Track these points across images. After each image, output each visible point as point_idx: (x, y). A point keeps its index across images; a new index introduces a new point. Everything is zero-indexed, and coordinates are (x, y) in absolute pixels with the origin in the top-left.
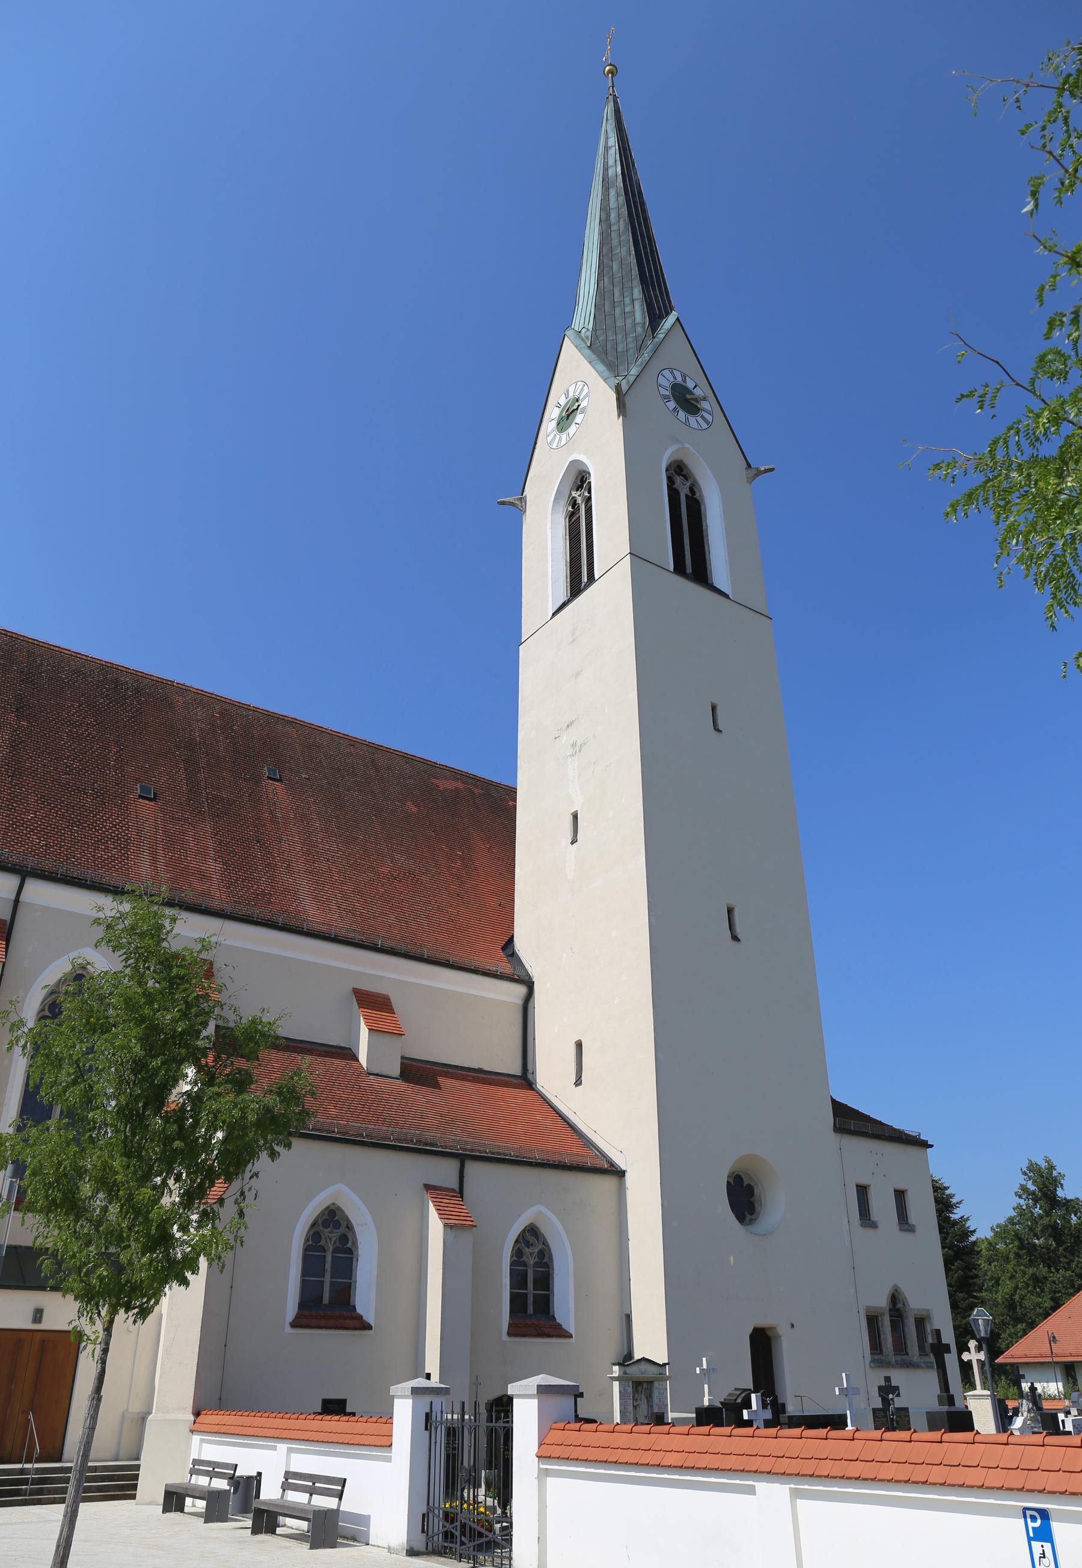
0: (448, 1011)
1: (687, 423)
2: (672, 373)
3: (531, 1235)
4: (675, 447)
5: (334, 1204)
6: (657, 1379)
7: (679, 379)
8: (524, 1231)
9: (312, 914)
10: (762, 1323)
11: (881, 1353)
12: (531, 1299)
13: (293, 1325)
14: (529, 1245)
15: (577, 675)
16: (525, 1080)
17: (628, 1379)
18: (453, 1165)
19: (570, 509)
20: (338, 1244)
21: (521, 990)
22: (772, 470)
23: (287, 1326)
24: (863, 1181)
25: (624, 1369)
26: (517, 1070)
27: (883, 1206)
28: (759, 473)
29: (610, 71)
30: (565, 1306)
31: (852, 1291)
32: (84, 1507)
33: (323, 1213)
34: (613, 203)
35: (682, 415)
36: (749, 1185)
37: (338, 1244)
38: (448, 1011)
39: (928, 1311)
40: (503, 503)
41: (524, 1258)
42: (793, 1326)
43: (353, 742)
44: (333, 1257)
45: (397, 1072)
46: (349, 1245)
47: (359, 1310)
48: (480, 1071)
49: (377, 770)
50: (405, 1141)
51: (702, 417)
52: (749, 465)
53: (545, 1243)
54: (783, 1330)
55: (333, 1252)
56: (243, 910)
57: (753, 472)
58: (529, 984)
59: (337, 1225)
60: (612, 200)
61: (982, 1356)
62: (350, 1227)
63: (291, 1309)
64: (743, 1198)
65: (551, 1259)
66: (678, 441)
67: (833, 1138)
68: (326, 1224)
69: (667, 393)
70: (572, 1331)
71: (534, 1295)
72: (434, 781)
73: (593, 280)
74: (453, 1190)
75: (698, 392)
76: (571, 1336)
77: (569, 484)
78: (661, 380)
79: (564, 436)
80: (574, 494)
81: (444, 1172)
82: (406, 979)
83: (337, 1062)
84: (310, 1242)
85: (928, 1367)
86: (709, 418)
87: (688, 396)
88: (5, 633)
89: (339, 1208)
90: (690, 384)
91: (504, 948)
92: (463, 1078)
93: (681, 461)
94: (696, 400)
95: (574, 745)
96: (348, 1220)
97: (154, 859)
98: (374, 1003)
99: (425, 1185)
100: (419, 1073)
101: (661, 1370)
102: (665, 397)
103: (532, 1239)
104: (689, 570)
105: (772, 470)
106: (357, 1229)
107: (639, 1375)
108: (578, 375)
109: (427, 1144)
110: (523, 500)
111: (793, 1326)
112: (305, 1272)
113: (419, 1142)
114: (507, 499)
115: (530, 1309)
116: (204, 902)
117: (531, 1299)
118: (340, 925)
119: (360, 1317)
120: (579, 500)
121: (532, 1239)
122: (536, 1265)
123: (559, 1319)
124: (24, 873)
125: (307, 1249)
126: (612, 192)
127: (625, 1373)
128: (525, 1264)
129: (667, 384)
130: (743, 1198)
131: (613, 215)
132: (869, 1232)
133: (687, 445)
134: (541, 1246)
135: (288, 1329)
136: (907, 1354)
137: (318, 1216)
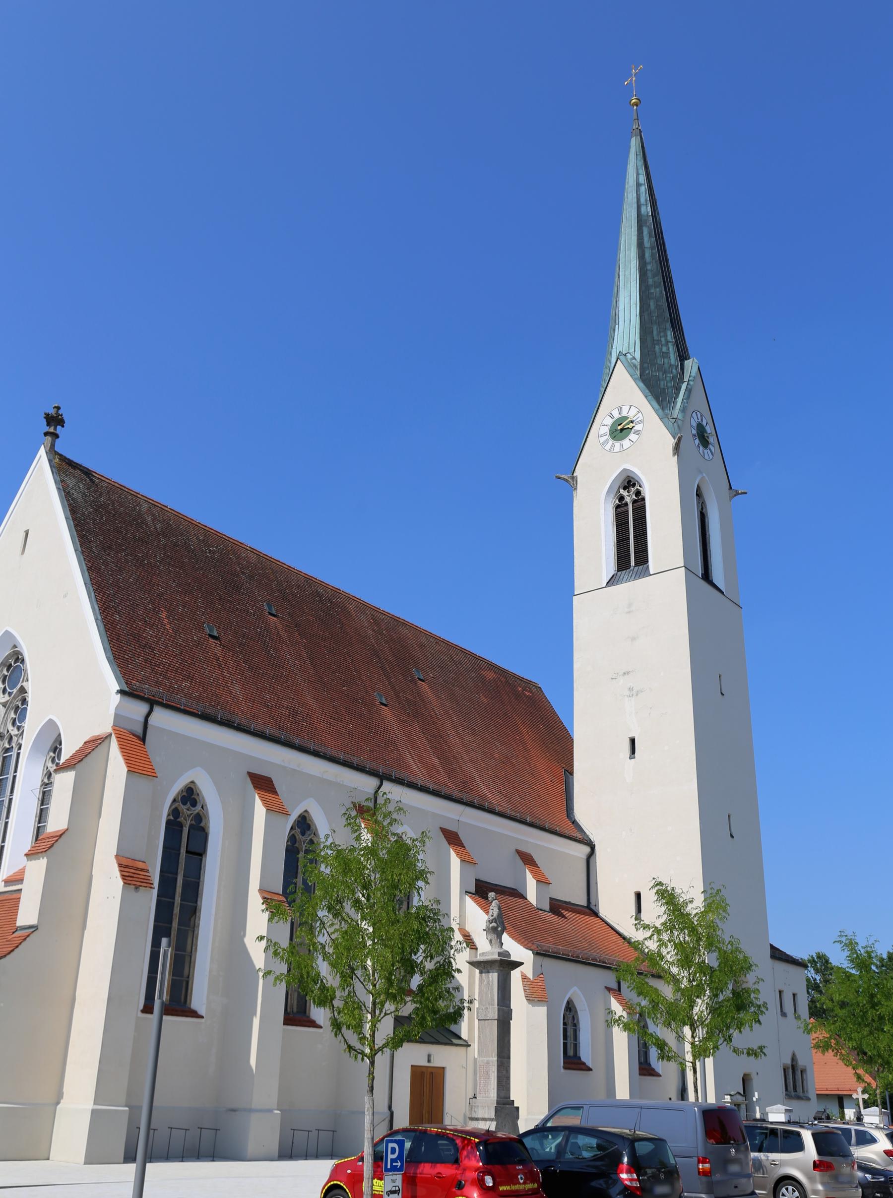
2: (702, 416)
9: (495, 800)
10: (747, 1071)
15: (633, 639)
16: (590, 910)
19: (617, 502)
21: (587, 850)
24: (781, 989)
26: (584, 903)
28: (737, 494)
32: (148, 1165)
34: (647, 244)
40: (559, 478)
45: (547, 908)
52: (731, 488)
54: (754, 1076)
58: (593, 848)
60: (646, 239)
63: (141, 1007)
73: (635, 310)
74: (614, 990)
77: (618, 484)
79: (617, 444)
80: (622, 491)
95: (631, 689)
99: (606, 987)
108: (624, 394)
110: (574, 479)
113: (600, 961)
114: (563, 476)
116: (322, 749)
119: (584, 1064)
120: (628, 499)
124: (383, 777)
126: (645, 231)
131: (648, 255)
132: (784, 1018)
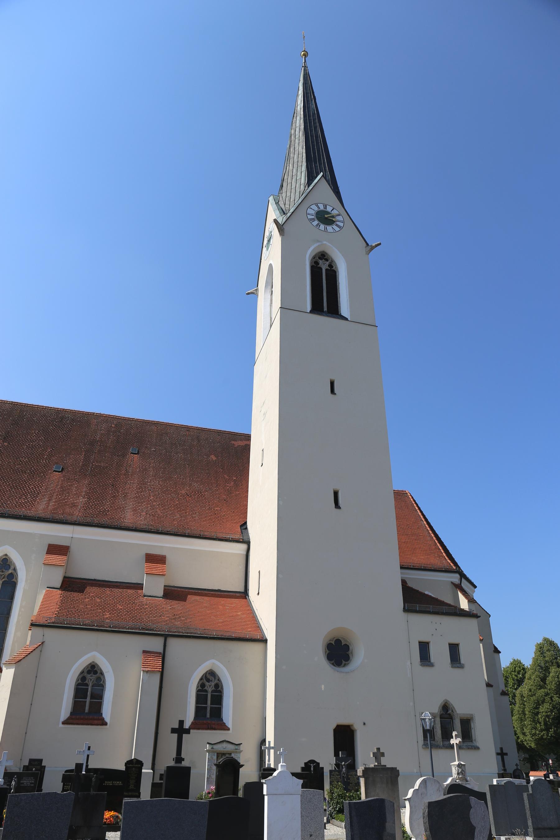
0: (199, 561)
1: (326, 230)
3: (211, 677)
4: (316, 245)
5: (93, 662)
6: (234, 752)
7: (316, 209)
8: (206, 673)
11: (434, 740)
12: (209, 709)
13: (64, 723)
14: (208, 680)
16: (245, 594)
17: (213, 752)
18: (161, 640)
20: (95, 682)
22: (380, 244)
23: (61, 723)
25: (211, 746)
26: (242, 589)
27: (440, 653)
28: (372, 248)
29: (304, 55)
30: (228, 714)
31: (412, 704)
33: (87, 666)
35: (322, 227)
36: (346, 645)
37: (95, 682)
38: (199, 561)
39: (472, 715)
40: (248, 294)
41: (206, 688)
42: (364, 724)
43: (188, 429)
44: (211, 695)
45: (161, 593)
46: (220, 689)
47: (104, 716)
48: (219, 591)
49: (199, 441)
50: (136, 629)
51: (337, 225)
52: (367, 244)
53: (219, 680)
55: (93, 686)
56: (89, 520)
57: (370, 248)
58: (248, 543)
59: (96, 673)
61: (459, 740)
62: (102, 673)
64: (338, 652)
65: (222, 688)
66: (318, 241)
67: (403, 616)
68: (89, 672)
69: (313, 217)
70: (230, 725)
71: (211, 708)
72: (233, 442)
74: (160, 653)
75: (335, 212)
76: (229, 729)
78: (310, 211)
81: (156, 644)
82: (176, 546)
83: (129, 591)
84: (200, 688)
85: (468, 748)
86: (341, 224)
87: (326, 216)
88: (4, 402)
89: (96, 664)
90: (329, 209)
91: (241, 526)
92: (206, 595)
93: (324, 251)
94: (333, 217)
96: (101, 670)
97: (50, 500)
98: (155, 559)
99: (144, 652)
100: (173, 593)
101: (237, 747)
102: (311, 219)
103: (211, 678)
104: (325, 309)
105: (380, 244)
106: (105, 674)
107: (222, 750)
109: (151, 630)
111: (364, 724)
112: (197, 702)
113: (143, 629)
115: (208, 715)
117: (209, 709)
118: (142, 522)
121: (211, 678)
122: (212, 691)
123: (225, 721)
125: (198, 691)
127: (212, 748)
128: (206, 691)
129: (313, 212)
130: (338, 652)
133: (325, 242)
134: (216, 681)
135: (61, 725)
136: (223, 727)
137: (84, 668)
